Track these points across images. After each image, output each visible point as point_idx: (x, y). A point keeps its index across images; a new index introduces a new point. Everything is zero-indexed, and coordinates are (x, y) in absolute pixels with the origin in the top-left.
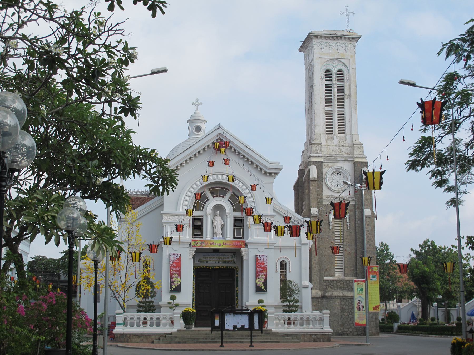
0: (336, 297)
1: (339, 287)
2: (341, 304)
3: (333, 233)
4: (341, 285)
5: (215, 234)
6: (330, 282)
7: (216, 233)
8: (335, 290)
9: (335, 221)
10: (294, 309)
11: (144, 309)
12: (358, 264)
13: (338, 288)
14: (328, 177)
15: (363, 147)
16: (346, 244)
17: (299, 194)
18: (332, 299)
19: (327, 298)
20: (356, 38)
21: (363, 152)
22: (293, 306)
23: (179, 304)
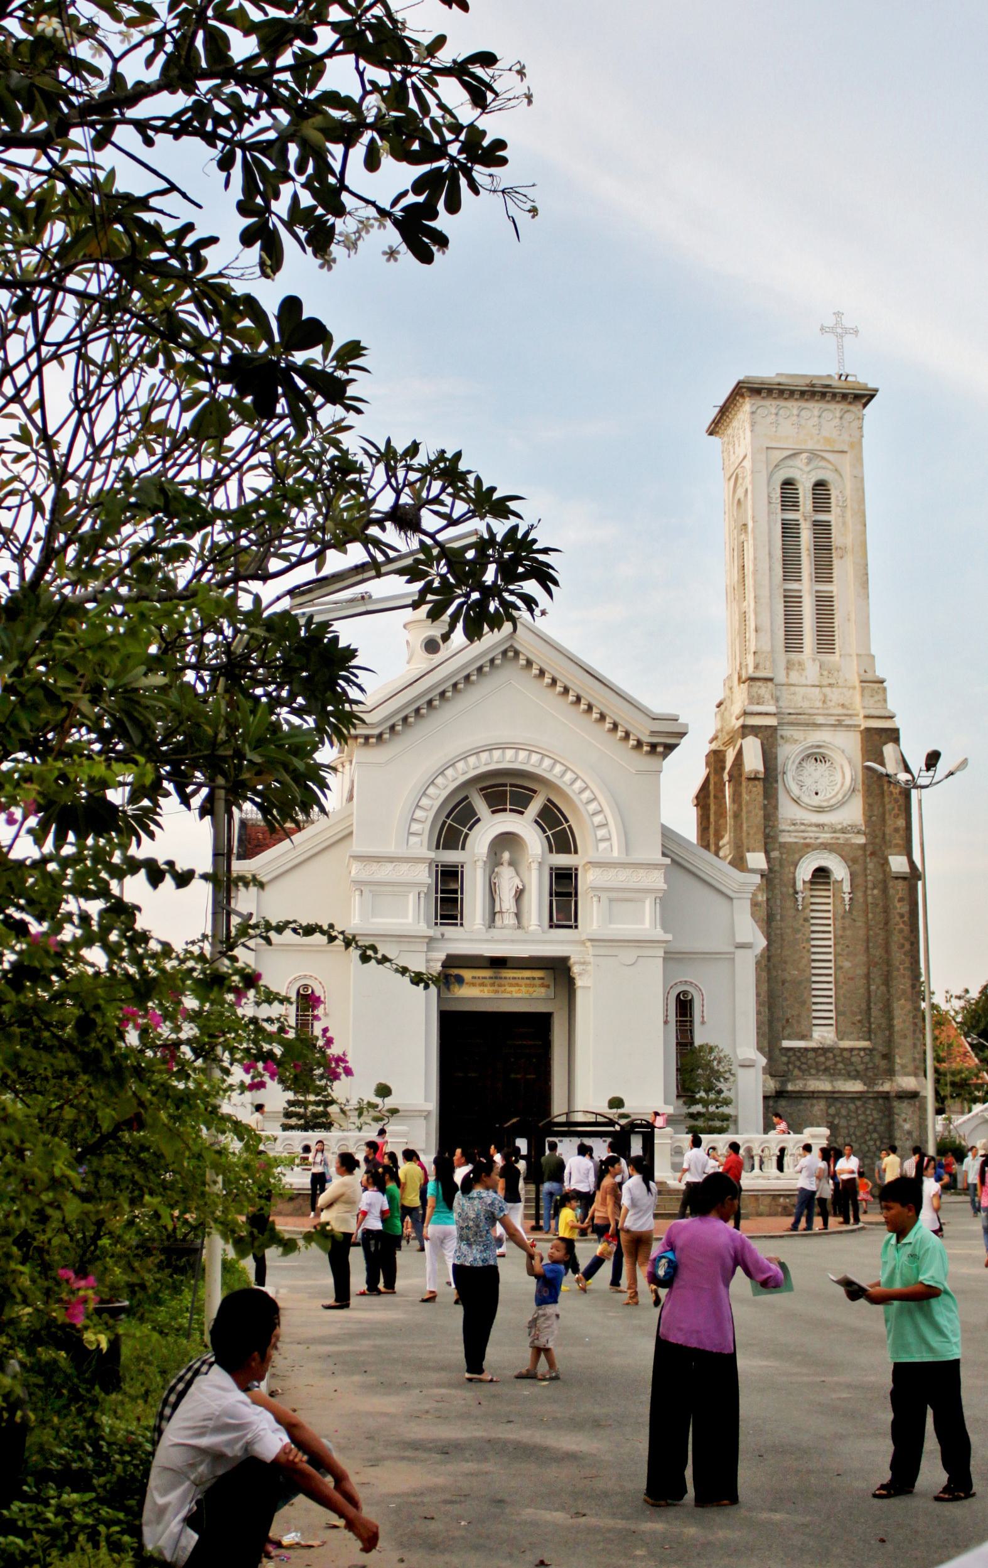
0: (814, 1095)
1: (823, 1067)
2: (828, 1115)
3: (806, 920)
4: (828, 1063)
5: (497, 916)
6: (798, 1054)
7: (501, 912)
8: (811, 1075)
9: (812, 890)
10: (718, 1124)
11: (302, 1122)
12: (872, 1005)
13: (818, 1070)
14: (791, 768)
15: (885, 689)
16: (843, 950)
17: (708, 818)
18: (804, 1101)
19: (790, 1097)
20: (864, 397)
21: (885, 701)
22: (713, 1117)
23: (400, 1108)
